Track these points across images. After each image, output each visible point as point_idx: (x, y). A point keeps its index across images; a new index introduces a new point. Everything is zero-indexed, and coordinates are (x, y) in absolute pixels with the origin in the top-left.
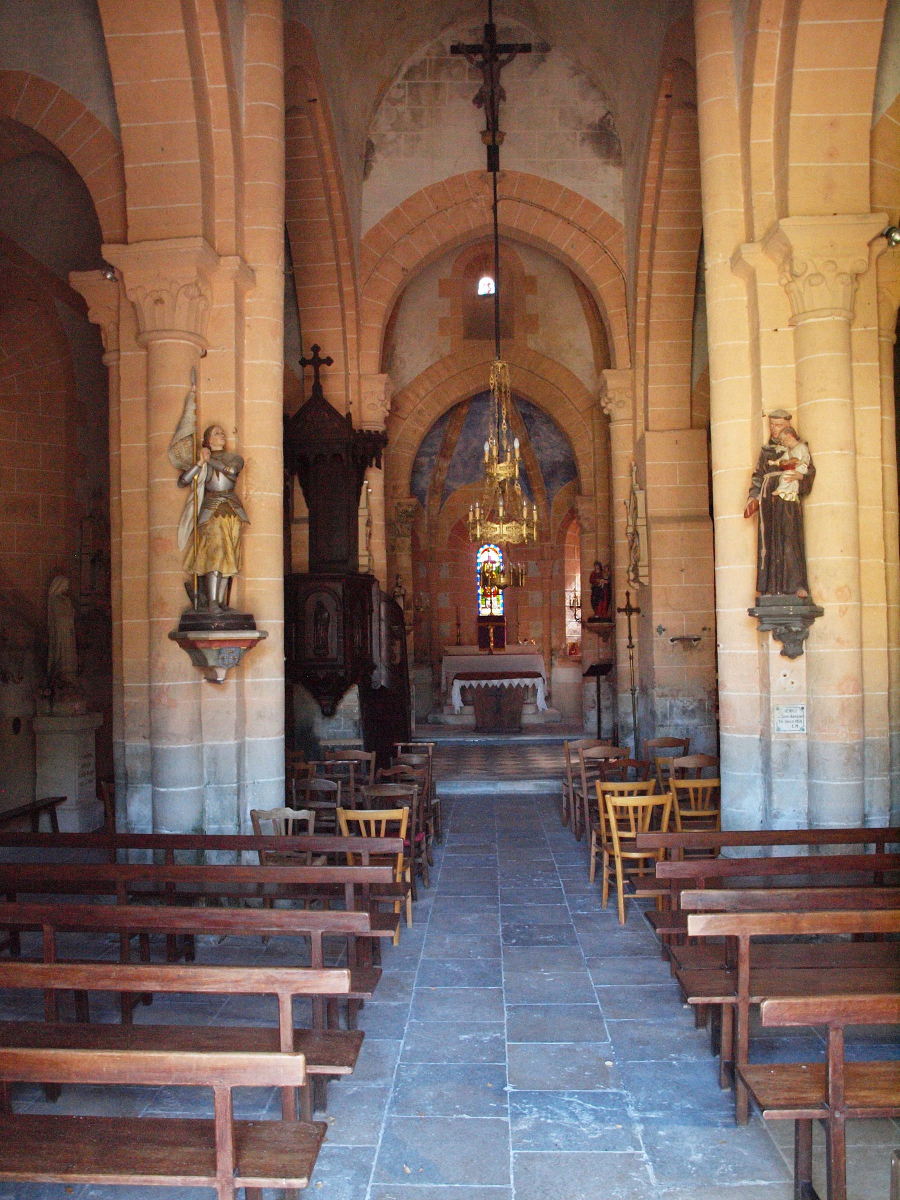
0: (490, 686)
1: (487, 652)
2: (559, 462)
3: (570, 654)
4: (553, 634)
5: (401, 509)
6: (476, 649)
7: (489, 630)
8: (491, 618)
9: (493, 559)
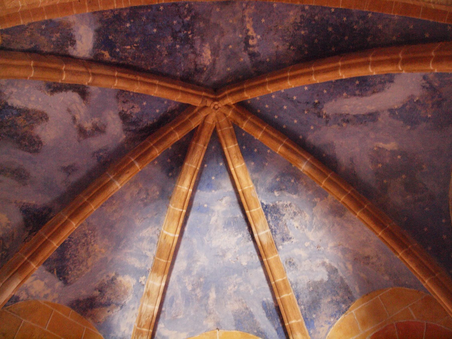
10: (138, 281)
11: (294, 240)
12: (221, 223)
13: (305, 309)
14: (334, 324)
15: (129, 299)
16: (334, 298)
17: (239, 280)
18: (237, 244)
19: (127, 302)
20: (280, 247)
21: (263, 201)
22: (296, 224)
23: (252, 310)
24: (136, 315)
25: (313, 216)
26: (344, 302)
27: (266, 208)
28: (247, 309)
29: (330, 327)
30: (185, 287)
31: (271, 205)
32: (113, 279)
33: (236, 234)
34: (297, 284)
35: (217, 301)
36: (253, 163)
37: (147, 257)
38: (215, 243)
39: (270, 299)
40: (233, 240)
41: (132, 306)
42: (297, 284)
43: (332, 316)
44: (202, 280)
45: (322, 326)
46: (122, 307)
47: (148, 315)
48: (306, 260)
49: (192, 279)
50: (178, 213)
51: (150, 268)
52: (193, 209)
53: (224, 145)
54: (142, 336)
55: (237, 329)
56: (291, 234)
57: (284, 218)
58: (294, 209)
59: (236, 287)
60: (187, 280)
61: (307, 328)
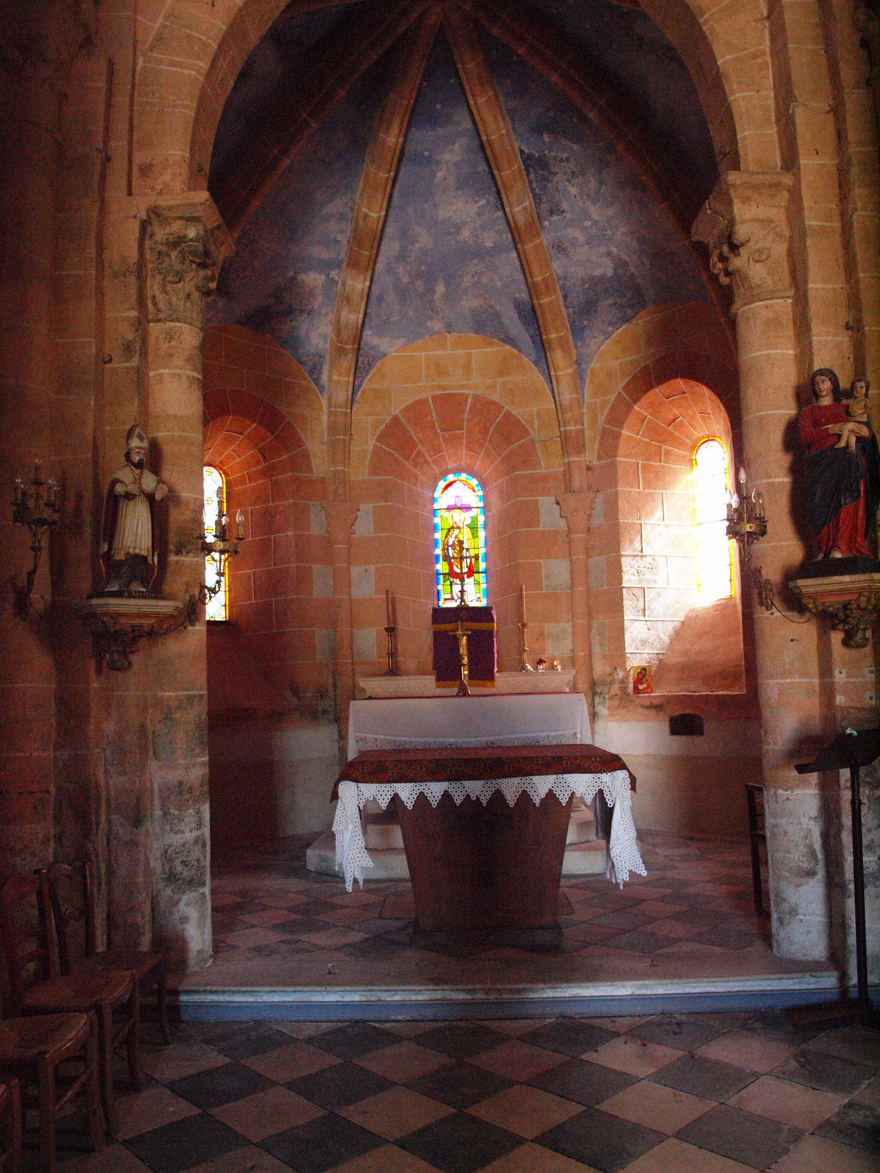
0: (458, 800)
1: (455, 691)
2: (601, 278)
3: (636, 690)
4: (597, 650)
5: (161, 233)
6: (428, 683)
7: (456, 640)
8: (464, 613)
9: (465, 502)
10: (328, 276)
11: (568, 216)
12: (451, 180)
13: (574, 313)
14: (611, 335)
15: (317, 302)
16: (619, 300)
17: (481, 268)
18: (479, 214)
19: (316, 307)
20: (546, 223)
21: (523, 148)
22: (574, 191)
23: (498, 308)
24: (331, 323)
25: (601, 183)
26: (632, 307)
27: (528, 161)
28: (491, 307)
29: (607, 339)
30: (399, 280)
31: (537, 155)
32: (293, 280)
33: (477, 198)
34: (566, 278)
35: (446, 296)
36: (509, 81)
37: (336, 242)
38: (444, 213)
39: (525, 296)
40: (473, 208)
41: (324, 311)
42: (566, 278)
43: (610, 324)
44: (423, 268)
45: (595, 337)
46: (308, 315)
47: (350, 327)
48: (583, 245)
49: (409, 267)
50: (383, 181)
51: (344, 256)
52: (405, 160)
53: (457, 60)
54: (346, 355)
55: (476, 333)
56: (565, 205)
57: (556, 179)
58: (572, 166)
59: (476, 278)
60: (401, 270)
61: (573, 338)
